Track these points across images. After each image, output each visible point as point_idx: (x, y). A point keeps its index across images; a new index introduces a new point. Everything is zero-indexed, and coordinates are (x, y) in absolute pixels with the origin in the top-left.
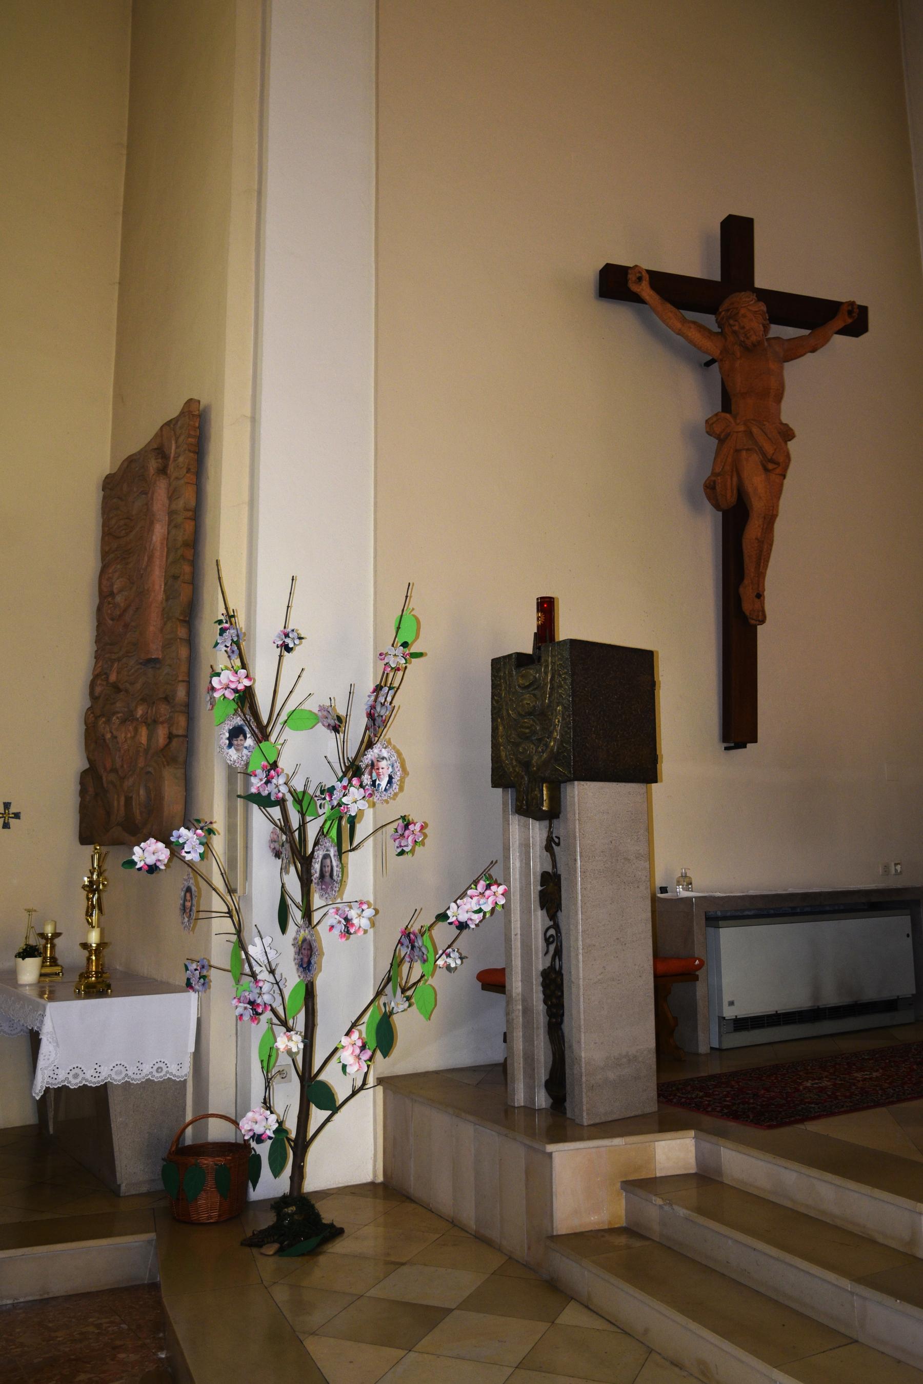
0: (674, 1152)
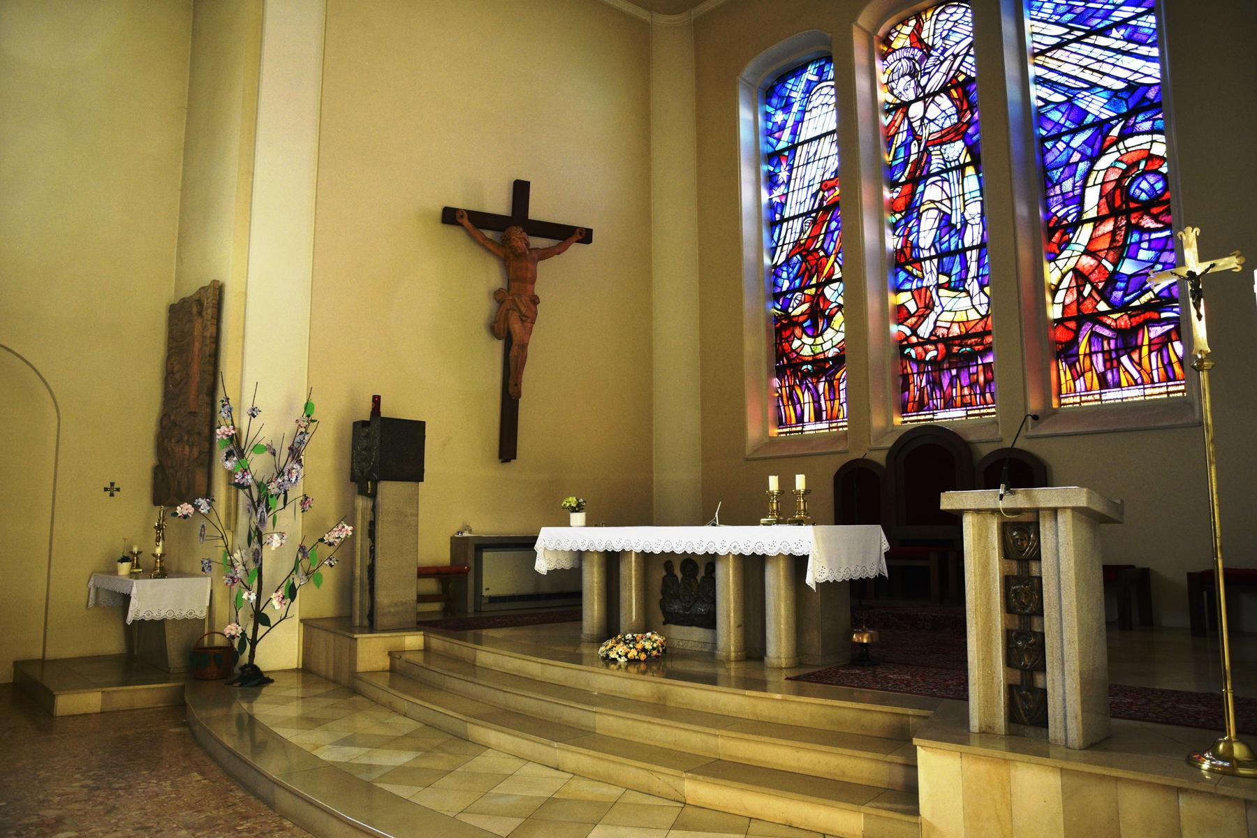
0: (413, 641)
